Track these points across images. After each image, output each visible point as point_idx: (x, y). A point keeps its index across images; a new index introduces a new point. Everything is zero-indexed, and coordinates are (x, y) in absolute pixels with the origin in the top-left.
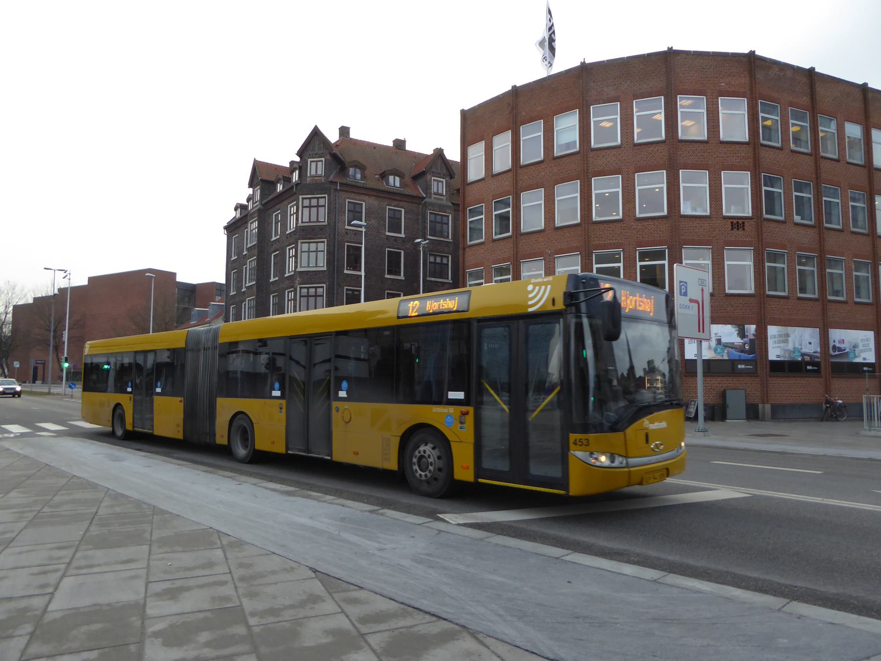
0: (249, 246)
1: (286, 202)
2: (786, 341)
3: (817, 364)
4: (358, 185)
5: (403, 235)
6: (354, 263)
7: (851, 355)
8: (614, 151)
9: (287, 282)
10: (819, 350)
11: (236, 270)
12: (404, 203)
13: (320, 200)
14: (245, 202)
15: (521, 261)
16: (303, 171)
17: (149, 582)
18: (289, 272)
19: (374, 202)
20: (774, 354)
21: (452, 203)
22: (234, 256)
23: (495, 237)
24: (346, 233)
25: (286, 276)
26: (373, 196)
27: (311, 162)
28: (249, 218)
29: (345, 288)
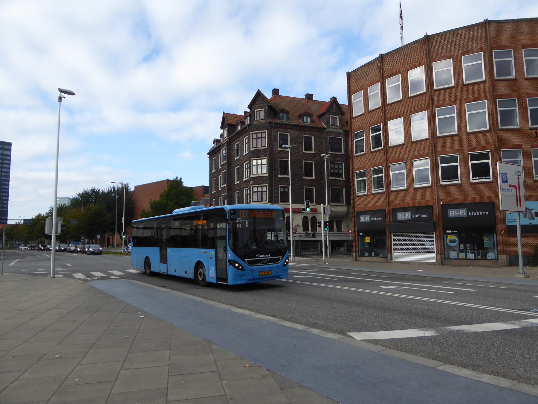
0: (222, 163)
1: (243, 136)
5: (313, 152)
6: (285, 171)
8: (450, 90)
9: (245, 184)
11: (215, 178)
12: (313, 132)
14: (219, 138)
15: (390, 164)
16: (252, 117)
18: (246, 178)
19: (295, 133)
21: (343, 131)
22: (214, 170)
23: (372, 150)
24: (279, 153)
25: (244, 180)
26: (294, 129)
27: (256, 111)
28: (221, 147)
29: (279, 186)
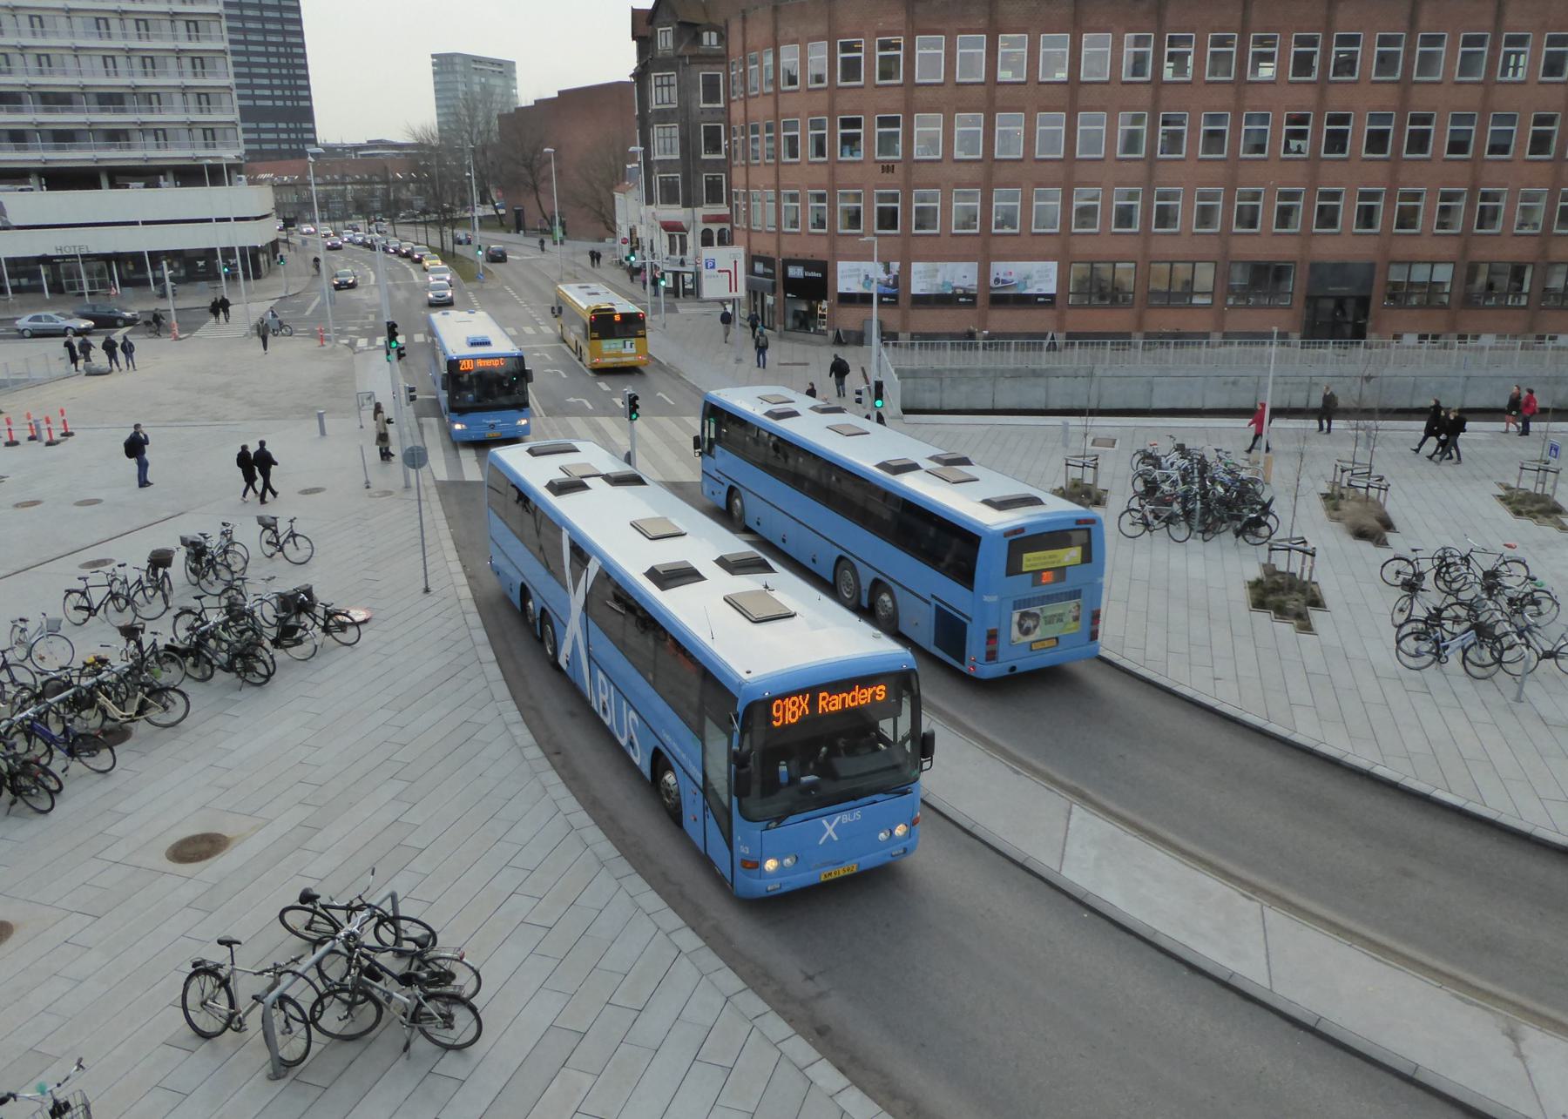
2: (935, 276)
3: (974, 297)
4: (712, 53)
7: (1021, 286)
10: (976, 283)
13: (671, 78)
17: (320, 417)
20: (918, 287)
24: (702, 113)
